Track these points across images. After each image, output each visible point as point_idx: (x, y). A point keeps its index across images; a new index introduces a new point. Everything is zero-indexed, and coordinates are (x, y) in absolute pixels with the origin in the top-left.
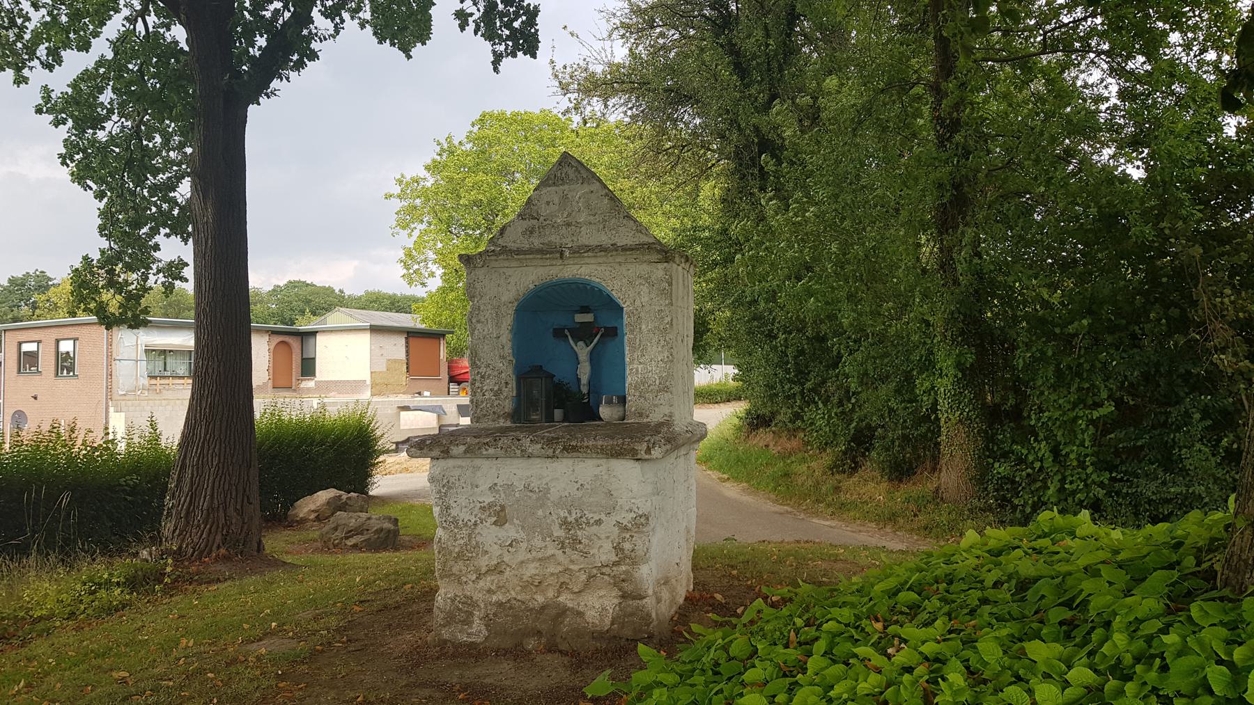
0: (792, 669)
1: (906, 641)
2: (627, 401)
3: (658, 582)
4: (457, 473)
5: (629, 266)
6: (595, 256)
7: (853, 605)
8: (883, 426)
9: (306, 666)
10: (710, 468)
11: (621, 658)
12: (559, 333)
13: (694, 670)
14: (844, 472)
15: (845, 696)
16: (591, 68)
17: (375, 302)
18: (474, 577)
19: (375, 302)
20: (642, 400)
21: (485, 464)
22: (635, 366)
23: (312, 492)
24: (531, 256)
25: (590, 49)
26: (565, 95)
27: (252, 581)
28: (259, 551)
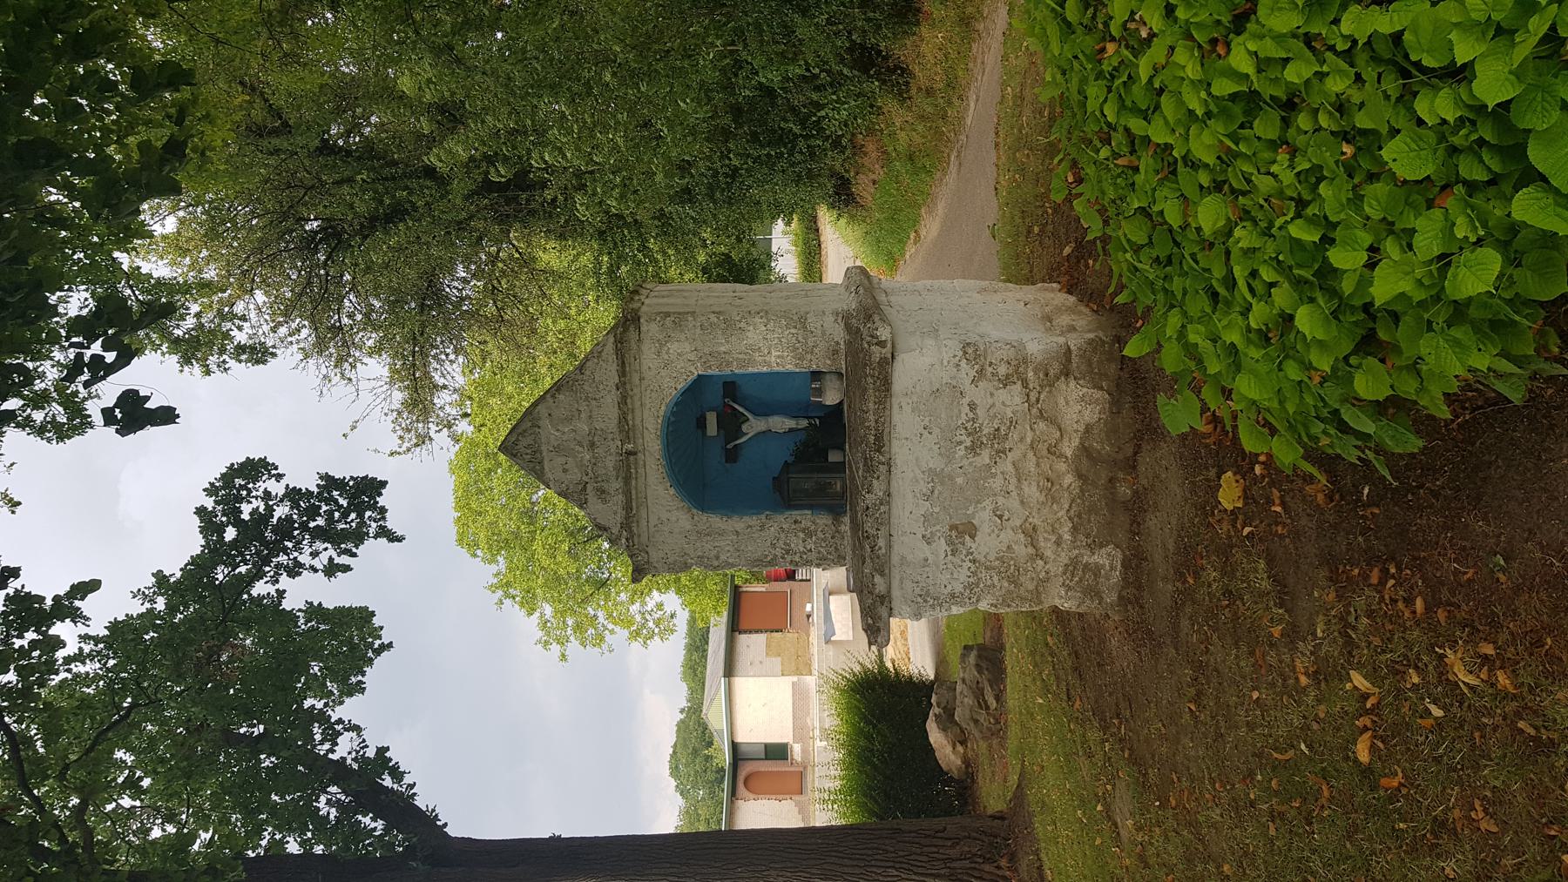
0: (1166, 163)
1: (1133, 13)
2: (818, 369)
3: (1048, 330)
4: (908, 585)
5: (645, 367)
6: (633, 412)
7: (1084, 81)
8: (850, 33)
9: (1150, 771)
10: (903, 255)
11: (1145, 378)
12: (732, 456)
13: (1165, 290)
14: (908, 83)
15: (1203, 94)
16: (396, 405)
17: (695, 671)
18: (1041, 563)
19: (695, 671)
20: (816, 350)
21: (898, 550)
22: (774, 359)
23: (929, 750)
24: (633, 492)
25: (372, 406)
26: (431, 439)
27: (1041, 827)
28: (1002, 818)
